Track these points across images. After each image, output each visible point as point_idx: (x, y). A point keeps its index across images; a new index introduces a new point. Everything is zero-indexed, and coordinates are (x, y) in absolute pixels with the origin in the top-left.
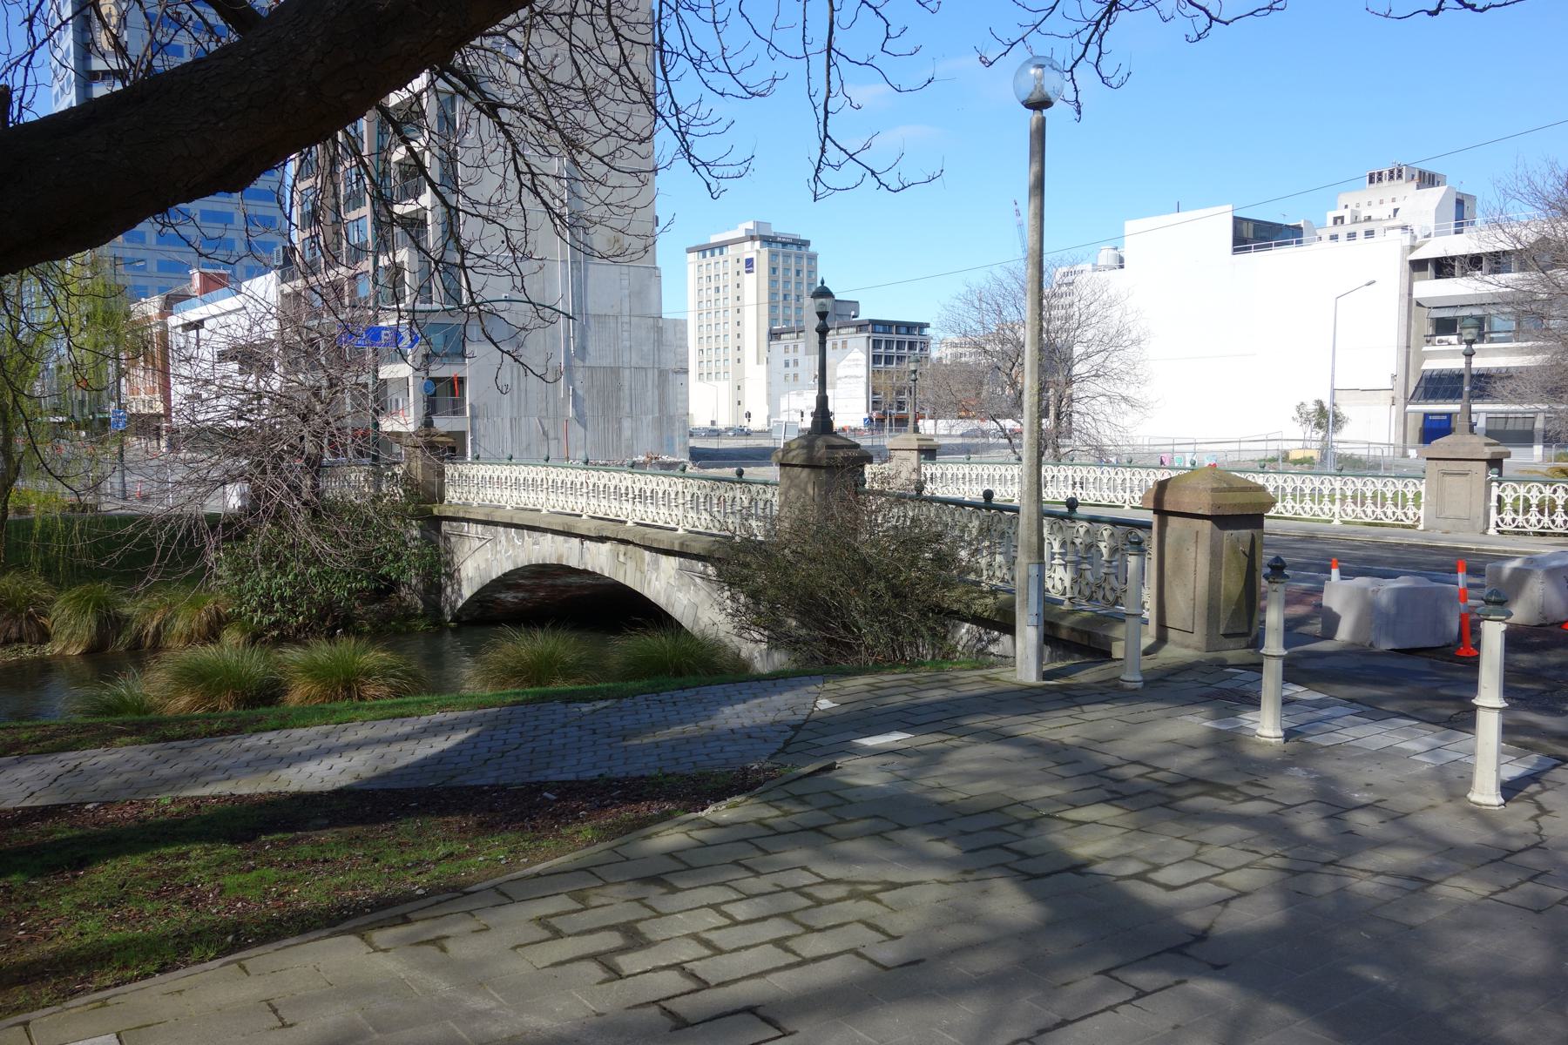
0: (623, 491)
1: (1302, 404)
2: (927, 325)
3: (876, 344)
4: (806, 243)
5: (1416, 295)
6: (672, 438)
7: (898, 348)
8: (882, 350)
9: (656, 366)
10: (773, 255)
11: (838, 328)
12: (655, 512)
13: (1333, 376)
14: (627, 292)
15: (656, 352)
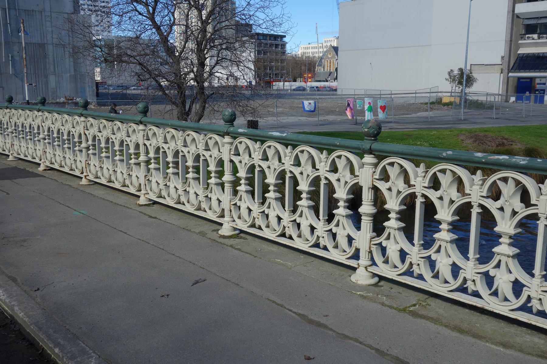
1: (452, 70)
5: (517, 11)
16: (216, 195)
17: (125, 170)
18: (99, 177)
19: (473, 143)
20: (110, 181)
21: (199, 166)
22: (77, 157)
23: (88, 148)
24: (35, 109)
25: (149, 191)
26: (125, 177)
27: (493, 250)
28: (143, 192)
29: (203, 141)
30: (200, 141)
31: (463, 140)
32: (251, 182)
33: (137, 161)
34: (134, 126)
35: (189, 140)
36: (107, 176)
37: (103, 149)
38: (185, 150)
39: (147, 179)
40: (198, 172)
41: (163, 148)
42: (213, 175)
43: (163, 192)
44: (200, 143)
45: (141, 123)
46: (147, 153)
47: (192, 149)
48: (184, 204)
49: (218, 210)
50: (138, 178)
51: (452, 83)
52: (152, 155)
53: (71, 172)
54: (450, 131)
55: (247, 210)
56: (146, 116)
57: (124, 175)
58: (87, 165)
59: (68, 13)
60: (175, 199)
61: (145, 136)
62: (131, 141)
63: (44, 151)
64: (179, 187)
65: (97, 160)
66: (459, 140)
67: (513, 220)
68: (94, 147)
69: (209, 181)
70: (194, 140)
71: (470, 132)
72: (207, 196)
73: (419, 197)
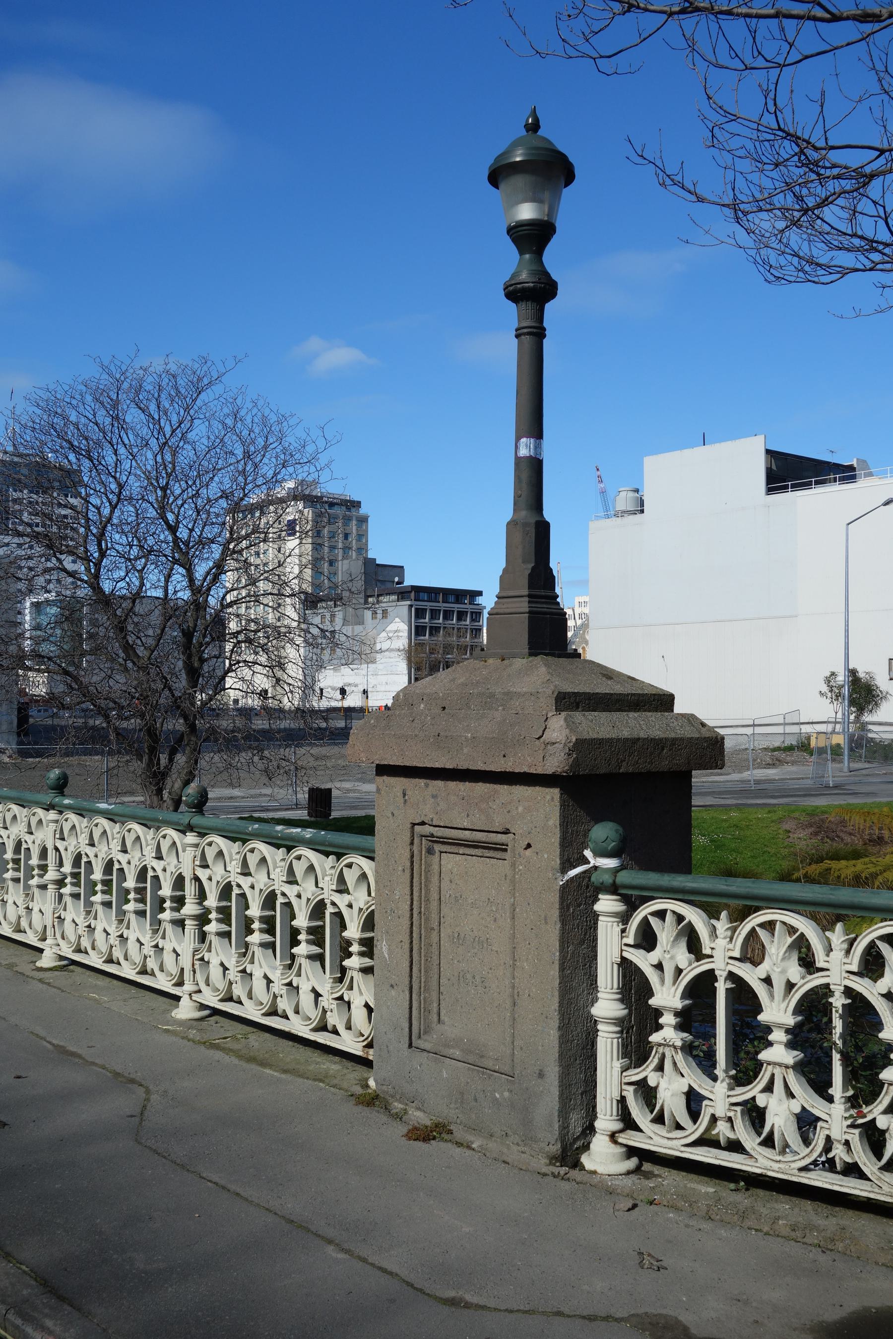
1: (833, 674)
2: (480, 593)
3: (420, 613)
4: (357, 504)
7: (445, 618)
8: (427, 620)
10: (318, 516)
11: (379, 596)
13: (847, 631)
16: (261, 967)
17: (115, 926)
18: (22, 929)
19: (811, 839)
20: (110, 961)
21: (274, 917)
22: (95, 918)
23: (60, 883)
25: (203, 986)
26: (20, 913)
27: (651, 1039)
28: (188, 987)
29: (283, 864)
30: (276, 863)
31: (789, 832)
32: (318, 939)
33: (176, 915)
34: (40, 812)
35: (253, 860)
36: (138, 959)
37: (9, 864)
38: (245, 882)
39: (200, 956)
40: (271, 931)
41: (239, 886)
42: (302, 937)
43: (236, 988)
44: (275, 867)
45: (190, 828)
46: (202, 895)
47: (218, 872)
48: (240, 1003)
50: (178, 955)
51: (835, 703)
52: (212, 901)
53: (322, 1038)
54: (769, 812)
55: (313, 995)
57: (79, 927)
58: (197, 962)
60: (104, 952)
61: (58, 832)
62: (33, 843)
63: (56, 915)
64: (231, 963)
65: (22, 892)
66: (781, 831)
67: (790, 1000)
68: (75, 878)
69: (295, 950)
70: (263, 860)
71: (812, 813)
72: (290, 984)
73: (837, 994)
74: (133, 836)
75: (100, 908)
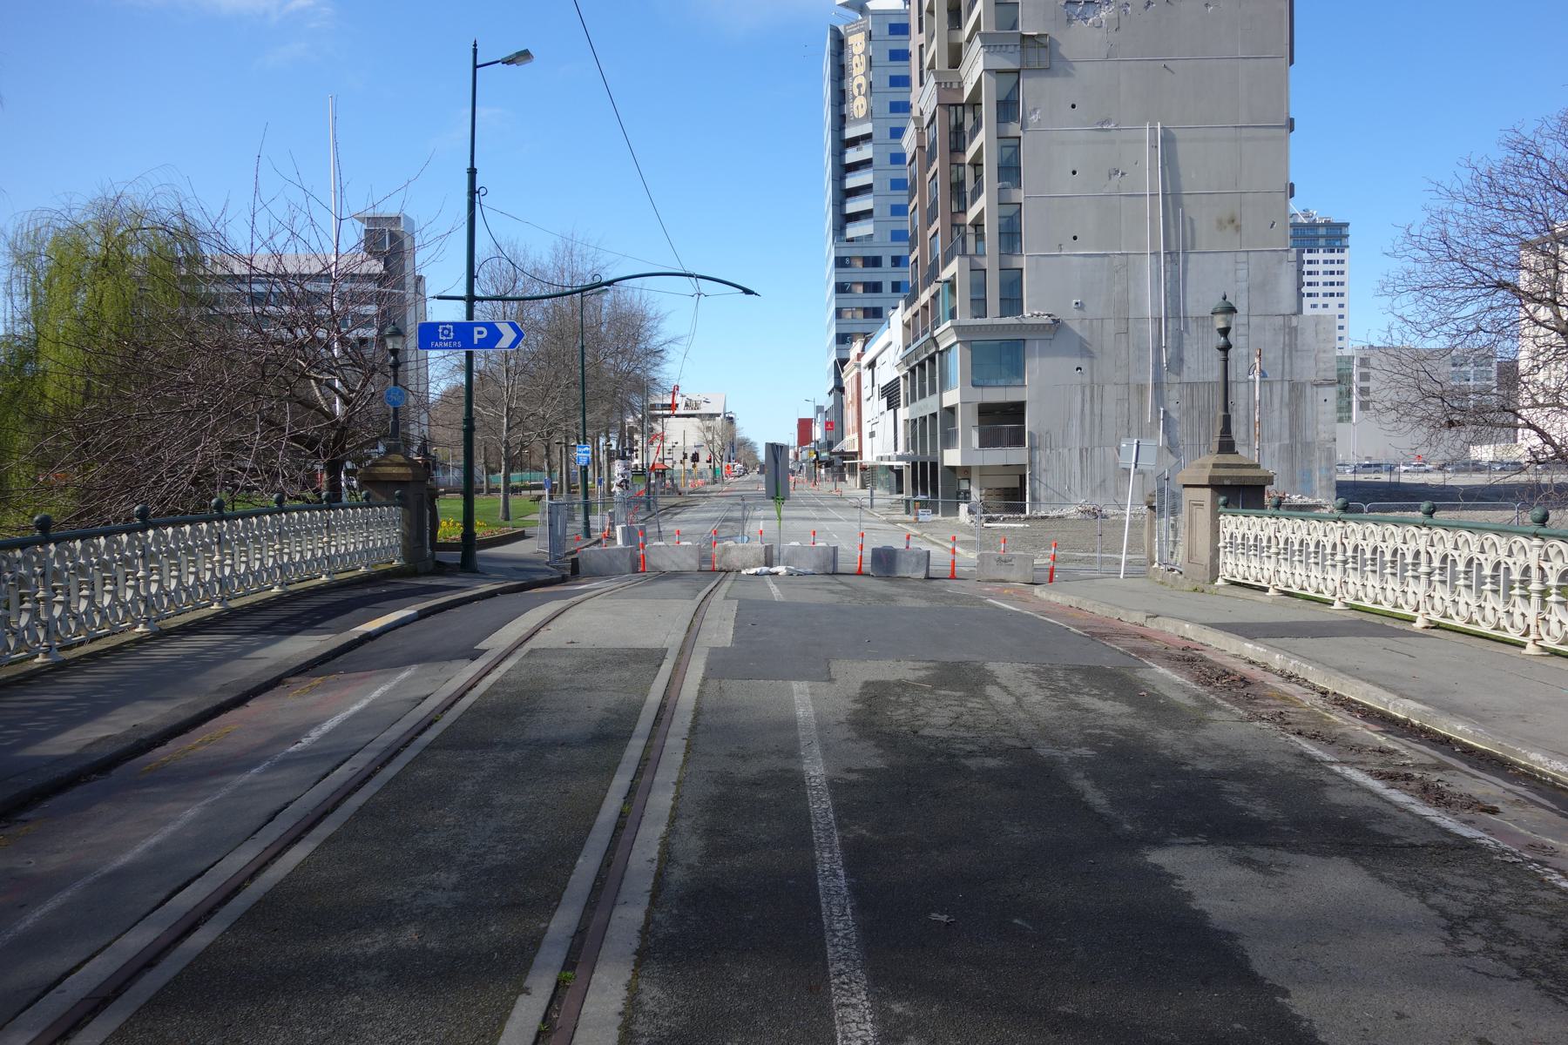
0: (1516, 575)
6: (1310, 471)
9: (1287, 377)
12: (1378, 586)
14: (1244, 285)
15: (1287, 361)
24: (1297, 517)
46: (1430, 561)
49: (1523, 627)
56: (1544, 526)
59: (1284, 315)
74: (1369, 530)
75: (1297, 563)
